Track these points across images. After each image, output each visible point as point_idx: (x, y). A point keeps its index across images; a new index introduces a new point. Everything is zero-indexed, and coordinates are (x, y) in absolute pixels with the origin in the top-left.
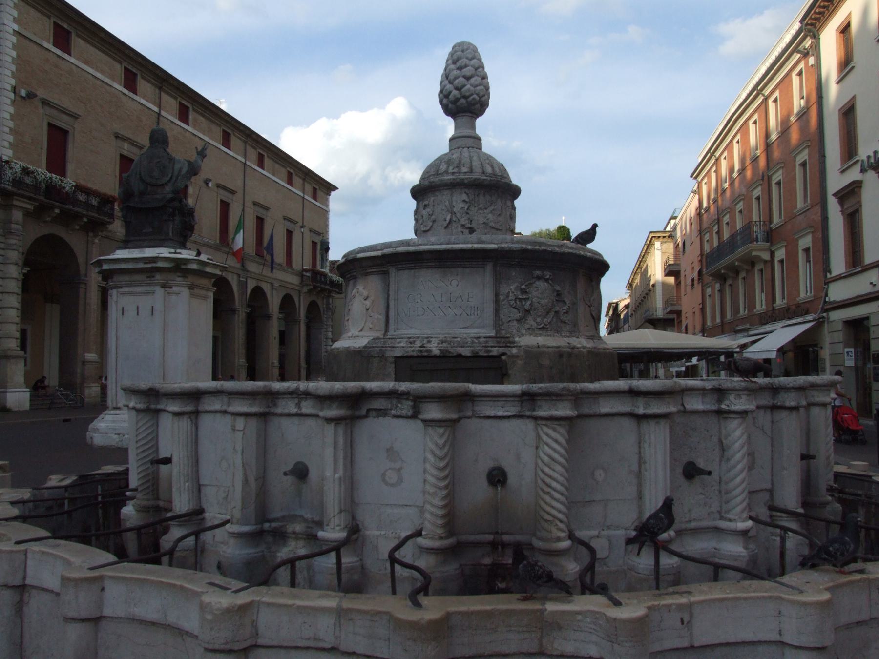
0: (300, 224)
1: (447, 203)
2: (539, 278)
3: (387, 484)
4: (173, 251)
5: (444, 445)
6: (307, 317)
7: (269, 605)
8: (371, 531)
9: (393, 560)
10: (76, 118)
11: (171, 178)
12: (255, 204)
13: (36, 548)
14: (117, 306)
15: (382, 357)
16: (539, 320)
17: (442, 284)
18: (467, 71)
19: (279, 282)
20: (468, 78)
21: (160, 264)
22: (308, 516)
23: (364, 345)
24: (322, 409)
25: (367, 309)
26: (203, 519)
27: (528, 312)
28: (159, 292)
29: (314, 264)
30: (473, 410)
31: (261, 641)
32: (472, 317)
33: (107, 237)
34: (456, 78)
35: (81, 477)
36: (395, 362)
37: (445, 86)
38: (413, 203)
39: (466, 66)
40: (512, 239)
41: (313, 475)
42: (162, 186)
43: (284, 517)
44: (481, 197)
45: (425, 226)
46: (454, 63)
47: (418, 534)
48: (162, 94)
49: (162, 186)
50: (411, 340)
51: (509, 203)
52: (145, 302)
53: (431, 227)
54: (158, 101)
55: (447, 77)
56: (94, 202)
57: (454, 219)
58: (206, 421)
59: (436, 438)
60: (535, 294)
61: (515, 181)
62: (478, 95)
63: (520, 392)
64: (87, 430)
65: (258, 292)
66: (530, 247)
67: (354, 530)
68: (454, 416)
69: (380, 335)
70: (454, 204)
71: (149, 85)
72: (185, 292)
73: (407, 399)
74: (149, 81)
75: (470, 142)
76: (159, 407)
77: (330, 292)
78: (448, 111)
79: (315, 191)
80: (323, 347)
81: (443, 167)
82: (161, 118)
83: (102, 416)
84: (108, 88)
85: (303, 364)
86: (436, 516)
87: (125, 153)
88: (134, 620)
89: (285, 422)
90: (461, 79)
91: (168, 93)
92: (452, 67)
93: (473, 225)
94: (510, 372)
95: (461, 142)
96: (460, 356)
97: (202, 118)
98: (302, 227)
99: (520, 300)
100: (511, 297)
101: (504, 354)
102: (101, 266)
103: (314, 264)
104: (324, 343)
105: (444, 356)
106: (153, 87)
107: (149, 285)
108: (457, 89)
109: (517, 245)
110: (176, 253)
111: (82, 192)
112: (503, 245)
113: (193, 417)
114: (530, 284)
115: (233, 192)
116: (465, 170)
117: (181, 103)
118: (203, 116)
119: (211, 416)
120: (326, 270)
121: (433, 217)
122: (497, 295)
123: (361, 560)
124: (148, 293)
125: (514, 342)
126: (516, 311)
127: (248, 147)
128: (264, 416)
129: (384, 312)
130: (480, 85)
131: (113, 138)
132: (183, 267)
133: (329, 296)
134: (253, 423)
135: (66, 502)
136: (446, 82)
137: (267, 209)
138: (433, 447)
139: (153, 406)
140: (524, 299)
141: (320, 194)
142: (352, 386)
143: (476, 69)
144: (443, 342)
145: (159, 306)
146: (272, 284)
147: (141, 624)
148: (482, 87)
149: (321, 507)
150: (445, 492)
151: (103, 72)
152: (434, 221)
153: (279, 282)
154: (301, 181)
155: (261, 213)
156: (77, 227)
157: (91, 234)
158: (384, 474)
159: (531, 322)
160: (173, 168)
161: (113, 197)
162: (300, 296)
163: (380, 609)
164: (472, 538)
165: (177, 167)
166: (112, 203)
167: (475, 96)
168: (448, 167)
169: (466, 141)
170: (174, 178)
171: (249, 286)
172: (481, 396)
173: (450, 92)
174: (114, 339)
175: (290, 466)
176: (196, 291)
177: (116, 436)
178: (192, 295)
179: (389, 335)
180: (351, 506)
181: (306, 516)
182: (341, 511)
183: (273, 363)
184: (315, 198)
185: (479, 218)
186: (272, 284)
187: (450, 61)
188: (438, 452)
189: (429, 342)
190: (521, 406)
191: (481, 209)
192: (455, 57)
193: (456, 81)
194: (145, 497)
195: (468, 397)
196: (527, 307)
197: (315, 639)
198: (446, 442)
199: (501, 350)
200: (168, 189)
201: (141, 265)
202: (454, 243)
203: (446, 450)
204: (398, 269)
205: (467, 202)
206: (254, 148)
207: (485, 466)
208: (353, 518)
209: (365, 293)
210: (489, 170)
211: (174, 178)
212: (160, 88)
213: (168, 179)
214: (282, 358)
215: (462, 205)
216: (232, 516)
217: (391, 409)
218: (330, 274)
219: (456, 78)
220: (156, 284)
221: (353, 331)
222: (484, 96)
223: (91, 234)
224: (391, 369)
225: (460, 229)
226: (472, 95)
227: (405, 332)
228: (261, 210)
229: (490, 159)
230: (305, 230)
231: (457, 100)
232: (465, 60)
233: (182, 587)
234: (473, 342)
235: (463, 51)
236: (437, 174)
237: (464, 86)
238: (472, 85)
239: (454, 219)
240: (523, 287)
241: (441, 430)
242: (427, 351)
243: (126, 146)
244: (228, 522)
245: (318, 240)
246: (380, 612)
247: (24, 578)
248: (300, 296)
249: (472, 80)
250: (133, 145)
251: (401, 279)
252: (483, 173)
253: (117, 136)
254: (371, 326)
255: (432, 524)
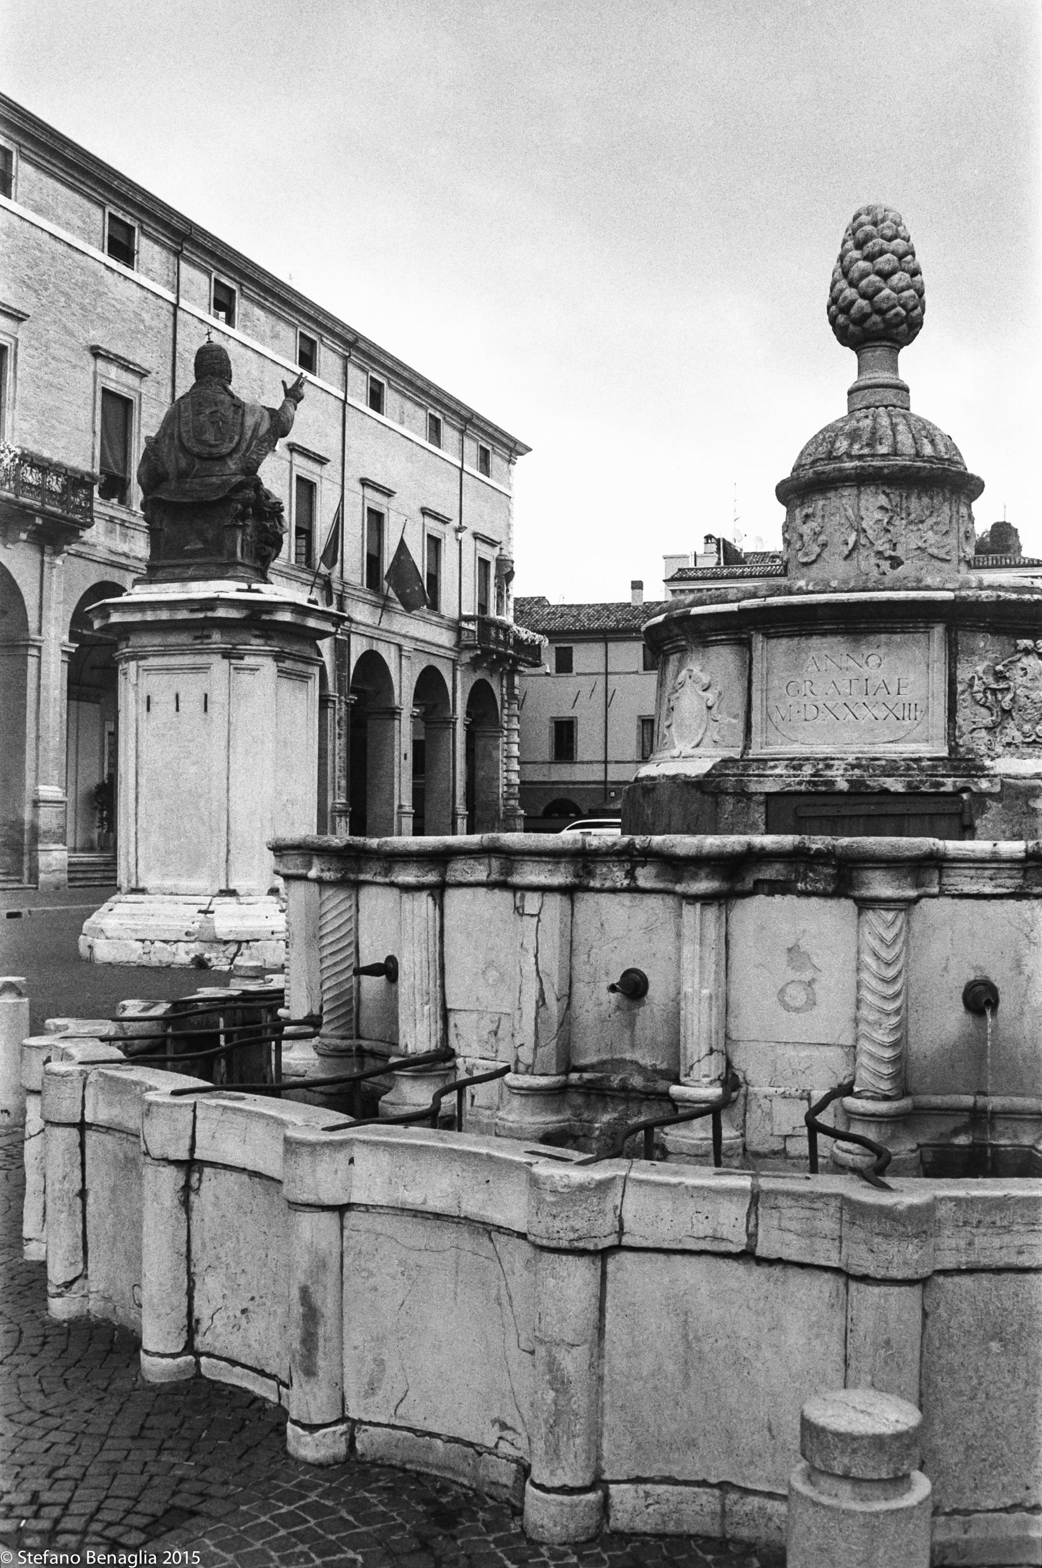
0: (455, 523)
1: (850, 512)
2: (1027, 652)
3: (787, 1008)
4: (244, 586)
5: (894, 941)
6: (468, 714)
7: (641, 1182)
8: (760, 1085)
9: (814, 1128)
10: (22, 320)
11: (238, 444)
12: (364, 482)
13: (213, 1102)
14: (137, 693)
15: (743, 795)
16: (1027, 727)
17: (851, 663)
18: (885, 262)
19: (411, 643)
20: (885, 276)
21: (221, 613)
22: (647, 1061)
23: (704, 771)
24: (679, 880)
25: (709, 708)
26: (455, 1068)
27: (1007, 713)
28: (219, 666)
29: (483, 607)
30: (940, 883)
31: (627, 1240)
32: (907, 722)
33: (78, 555)
34: (864, 275)
35: (176, 1005)
36: (766, 803)
37: (842, 291)
38: (780, 512)
39: (882, 252)
40: (981, 582)
41: (657, 992)
42: (222, 458)
43: (604, 1063)
44: (913, 499)
45: (806, 554)
46: (859, 246)
47: (845, 1090)
48: (183, 265)
49: (222, 458)
50: (796, 763)
51: (963, 510)
52: (192, 687)
53: (819, 555)
54: (172, 277)
55: (845, 274)
56: (55, 484)
57: (863, 541)
58: (454, 898)
59: (881, 930)
60: (1020, 680)
61: (973, 468)
62: (903, 306)
63: (1023, 854)
64: (79, 931)
65: (372, 661)
66: (1014, 596)
67: (731, 1081)
68: (912, 893)
69: (735, 753)
70: (863, 513)
71: (157, 248)
72: (269, 666)
73: (826, 865)
74: (156, 241)
75: (890, 396)
76: (362, 877)
77: (517, 661)
78: (844, 337)
79: (484, 458)
80: (502, 774)
81: (842, 445)
82: (179, 313)
83: (106, 906)
84: (77, 256)
85: (461, 808)
86: (880, 1060)
87: (112, 386)
88: (403, 1209)
89: (604, 899)
90: (873, 278)
91: (189, 261)
92: (856, 254)
93: (900, 553)
94: (978, 822)
95: (872, 397)
96: (885, 792)
97: (258, 312)
98: (459, 530)
99: (994, 691)
100: (978, 686)
101: (966, 789)
102: (108, 616)
103: (483, 607)
104: (502, 767)
105: (858, 791)
106: (165, 253)
107: (200, 652)
108: (864, 296)
109: (989, 592)
110: (250, 590)
111: (33, 466)
112: (963, 593)
113: (437, 892)
114: (1011, 662)
115: (321, 461)
116: (883, 450)
117: (217, 281)
118: (263, 307)
119: (468, 892)
120: (508, 618)
121: (822, 538)
122: (952, 682)
123: (743, 1135)
124: (197, 669)
125: (983, 768)
126: (983, 710)
127: (352, 370)
128: (568, 891)
129: (742, 713)
130: (908, 287)
131: (88, 356)
132: (265, 617)
133: (513, 672)
134: (555, 903)
135: (222, 1037)
136: (843, 284)
137: (389, 493)
138: (876, 944)
139: (352, 876)
140: (1001, 690)
141: (496, 461)
142: (734, 842)
143: (901, 257)
144: (853, 767)
145: (218, 697)
146: (400, 647)
147: (415, 1216)
148: (912, 292)
149: (675, 1046)
150: (894, 1020)
151: (67, 225)
152: (824, 545)
153: (411, 643)
154: (456, 435)
155: (376, 500)
156: (23, 536)
157: (48, 549)
158: (782, 991)
159: (1012, 732)
160: (242, 424)
161: (90, 475)
162: (454, 671)
163: (825, 1190)
164: (937, 1100)
165: (250, 421)
166: (89, 487)
167: (899, 309)
168: (851, 445)
169: (880, 396)
170: (244, 446)
171: (353, 649)
172: (956, 860)
173: (852, 303)
174: (132, 753)
175: (616, 979)
176: (288, 664)
177: (139, 944)
178: (283, 673)
179: (752, 754)
180: (725, 1046)
181: (642, 1062)
182: (711, 1051)
183: (400, 807)
184: (486, 471)
185: (909, 540)
186: (400, 647)
187: (850, 244)
188: (884, 954)
189: (829, 767)
190: (1024, 877)
191: (911, 523)
192: (860, 235)
193: (864, 283)
194: (340, 1033)
195: (937, 862)
196: (1006, 704)
197: (715, 1238)
198: (897, 935)
199: (960, 782)
200: (232, 465)
201: (182, 615)
202: (873, 590)
203: (897, 949)
204: (768, 636)
205: (887, 510)
206: (363, 369)
207: (962, 976)
208: (729, 1064)
209: (705, 679)
210: (928, 450)
211: (244, 446)
212: (178, 254)
213: (233, 445)
214: (419, 795)
215: (879, 515)
216: (517, 1061)
217: (797, 881)
218: (515, 627)
219: (864, 275)
220: (213, 652)
221: (682, 747)
222: (915, 307)
223: (48, 549)
224: (758, 815)
225: (873, 560)
226: (894, 307)
227: (784, 749)
228: (378, 497)
229: (926, 431)
230: (466, 536)
231: (866, 316)
232: (881, 241)
233: (490, 1157)
234: (909, 768)
235: (875, 224)
236: (830, 457)
237: (880, 290)
238: (893, 289)
239: (863, 541)
240: (999, 668)
241: (890, 916)
242: (826, 783)
243: (113, 371)
244: (507, 1070)
245: (490, 554)
246: (822, 1196)
247: (192, 1149)
248: (454, 671)
249: (895, 278)
250: (127, 369)
251: (773, 654)
252: (918, 454)
253: (96, 352)
254: (716, 737)
255: (874, 1074)
